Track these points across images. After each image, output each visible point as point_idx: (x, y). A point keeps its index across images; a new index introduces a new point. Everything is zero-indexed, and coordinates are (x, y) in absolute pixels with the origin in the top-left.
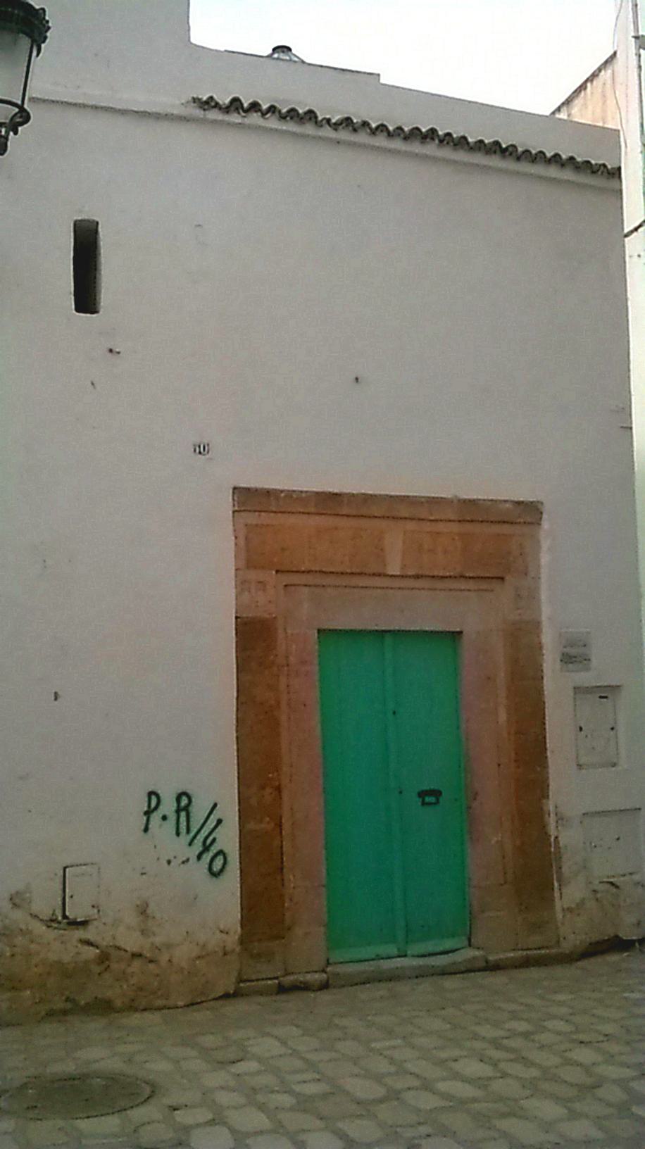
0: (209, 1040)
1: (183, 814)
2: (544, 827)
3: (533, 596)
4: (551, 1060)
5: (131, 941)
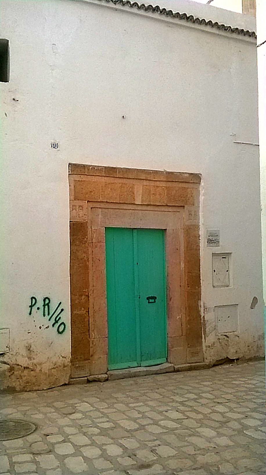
0: (57, 404)
1: (46, 307)
2: (199, 312)
3: (196, 215)
4: (206, 411)
5: (23, 362)
